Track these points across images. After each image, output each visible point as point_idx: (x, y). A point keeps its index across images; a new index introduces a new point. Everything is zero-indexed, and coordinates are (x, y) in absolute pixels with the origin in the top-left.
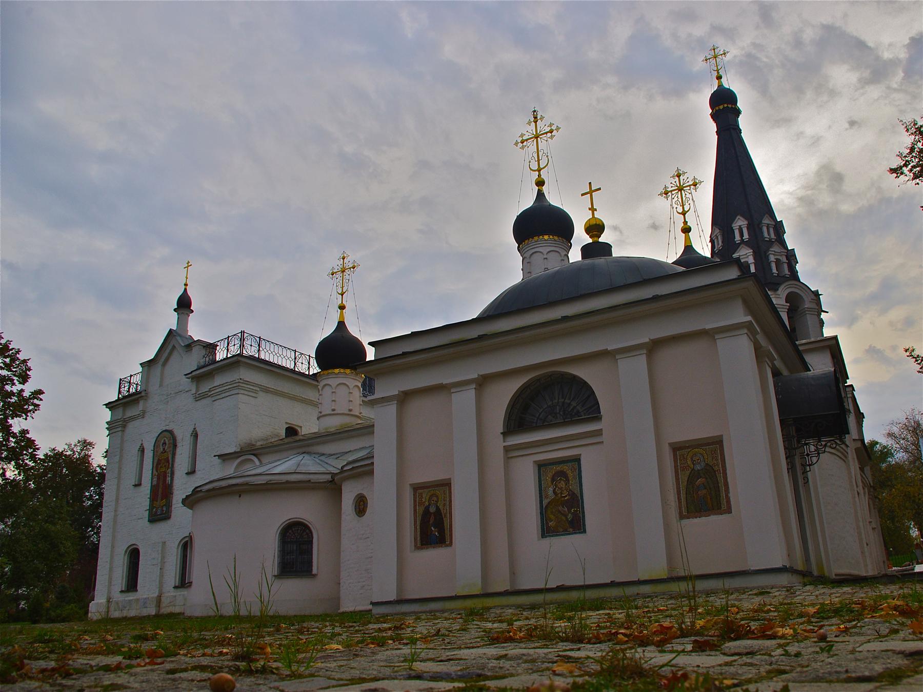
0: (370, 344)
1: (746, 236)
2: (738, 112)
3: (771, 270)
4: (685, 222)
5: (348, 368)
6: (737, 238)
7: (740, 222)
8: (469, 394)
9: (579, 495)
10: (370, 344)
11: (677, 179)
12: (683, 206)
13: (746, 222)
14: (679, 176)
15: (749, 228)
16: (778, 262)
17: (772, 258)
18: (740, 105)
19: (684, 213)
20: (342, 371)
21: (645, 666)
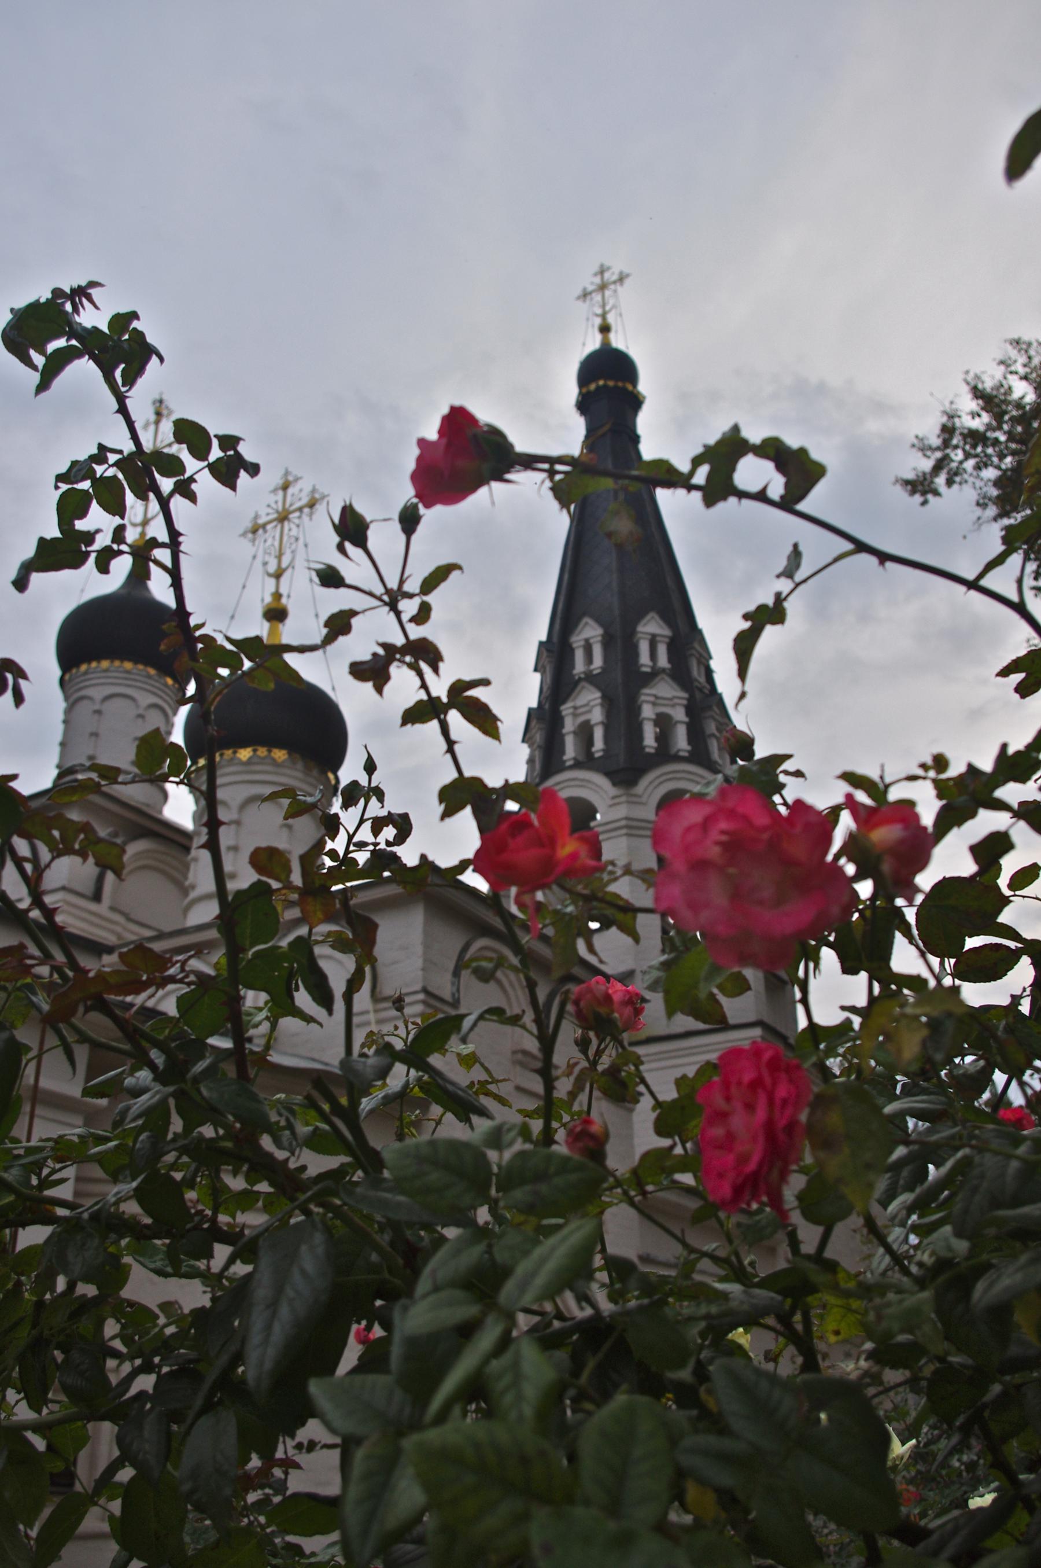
0: (216, 436)
1: (598, 661)
2: (636, 402)
3: (641, 738)
4: (277, 596)
5: (280, 747)
6: (644, 658)
7: (652, 626)
8: (288, 1023)
9: (141, 1259)
10: (216, 436)
11: (281, 493)
12: (279, 557)
13: (667, 632)
14: (285, 487)
15: (607, 642)
16: (663, 722)
17: (648, 712)
18: (643, 386)
19: (278, 575)
20: (262, 752)
21: (818, 1539)
